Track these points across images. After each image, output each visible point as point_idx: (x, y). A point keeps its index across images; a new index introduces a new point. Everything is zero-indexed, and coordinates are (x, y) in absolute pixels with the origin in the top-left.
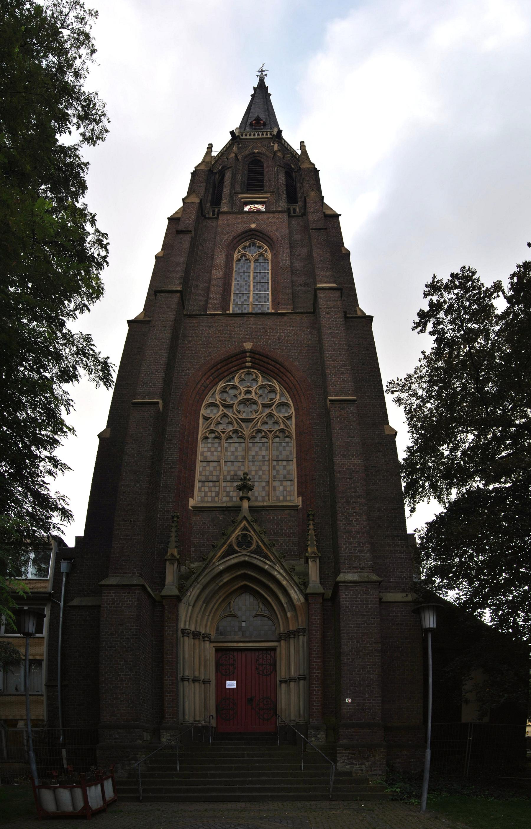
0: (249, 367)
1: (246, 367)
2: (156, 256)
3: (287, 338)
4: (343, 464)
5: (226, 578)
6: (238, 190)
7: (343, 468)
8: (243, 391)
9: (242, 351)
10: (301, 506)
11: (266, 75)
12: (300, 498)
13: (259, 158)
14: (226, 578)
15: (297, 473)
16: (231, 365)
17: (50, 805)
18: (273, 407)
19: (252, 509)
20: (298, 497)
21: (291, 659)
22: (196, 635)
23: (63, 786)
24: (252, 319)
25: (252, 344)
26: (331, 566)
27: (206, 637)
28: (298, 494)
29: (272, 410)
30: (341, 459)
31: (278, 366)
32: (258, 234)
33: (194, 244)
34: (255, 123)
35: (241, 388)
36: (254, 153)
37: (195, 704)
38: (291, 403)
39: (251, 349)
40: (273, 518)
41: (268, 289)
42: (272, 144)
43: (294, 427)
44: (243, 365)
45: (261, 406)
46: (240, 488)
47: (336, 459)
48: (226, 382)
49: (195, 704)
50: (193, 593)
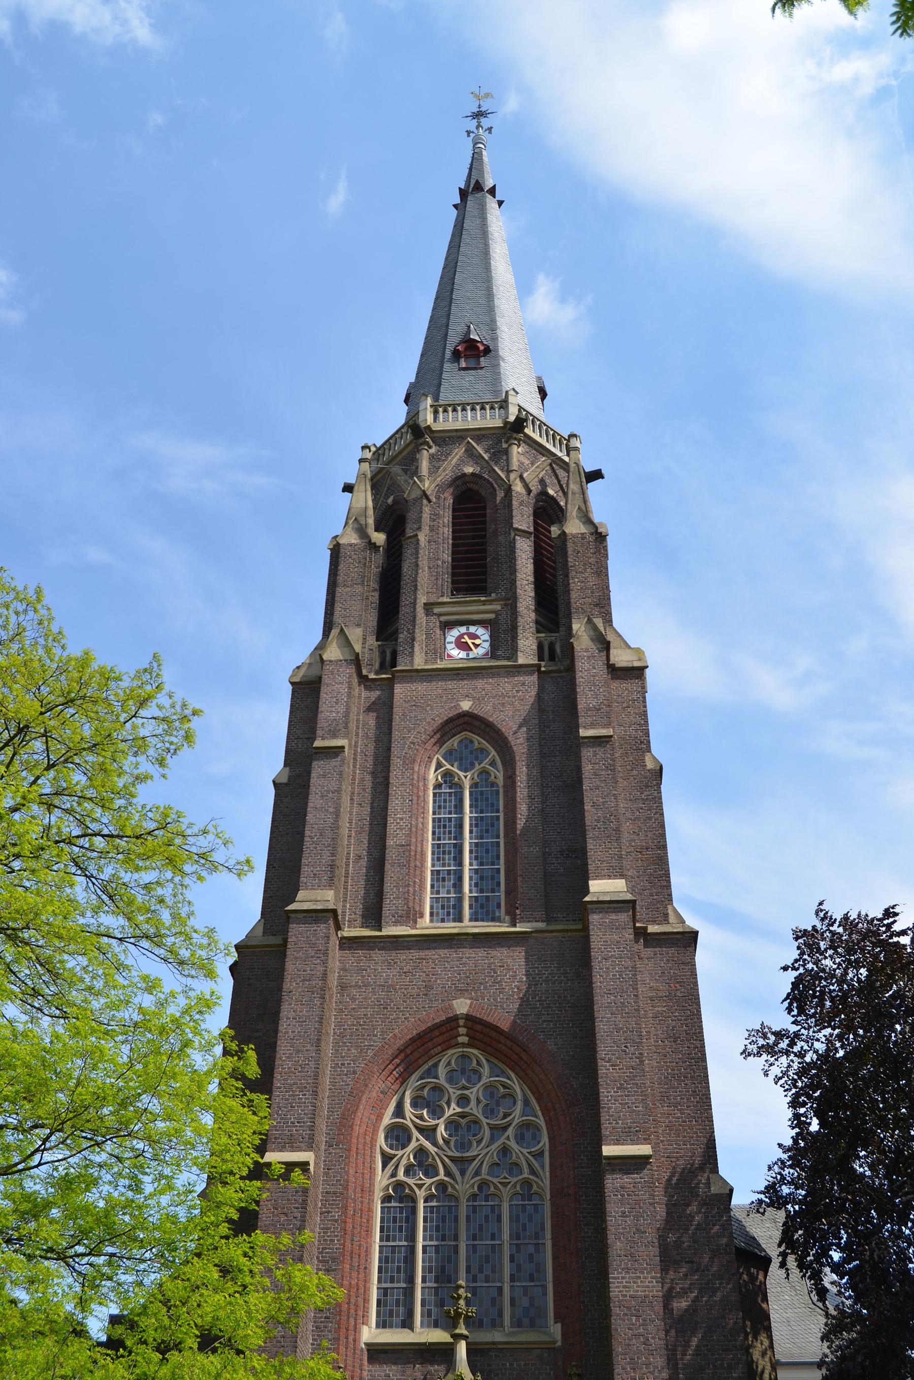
0: (463, 1045)
1: (457, 1045)
2: (274, 782)
4: (625, 1287)
7: (626, 1296)
8: (453, 1097)
9: (451, 1018)
10: (559, 1344)
11: (490, 129)
12: (559, 1325)
13: (475, 487)
15: (554, 1272)
16: (430, 1044)
18: (510, 1131)
20: (556, 1322)
25: (468, 1002)
28: (555, 1318)
29: (508, 1138)
30: (623, 1278)
31: (517, 1049)
32: (477, 723)
34: (466, 349)
35: (451, 1090)
36: (464, 475)
38: (542, 1122)
39: (467, 1015)
40: (511, 1365)
41: (498, 858)
42: (505, 446)
43: (548, 1174)
44: (453, 1042)
45: (486, 1128)
47: (614, 1278)
48: (421, 1078)
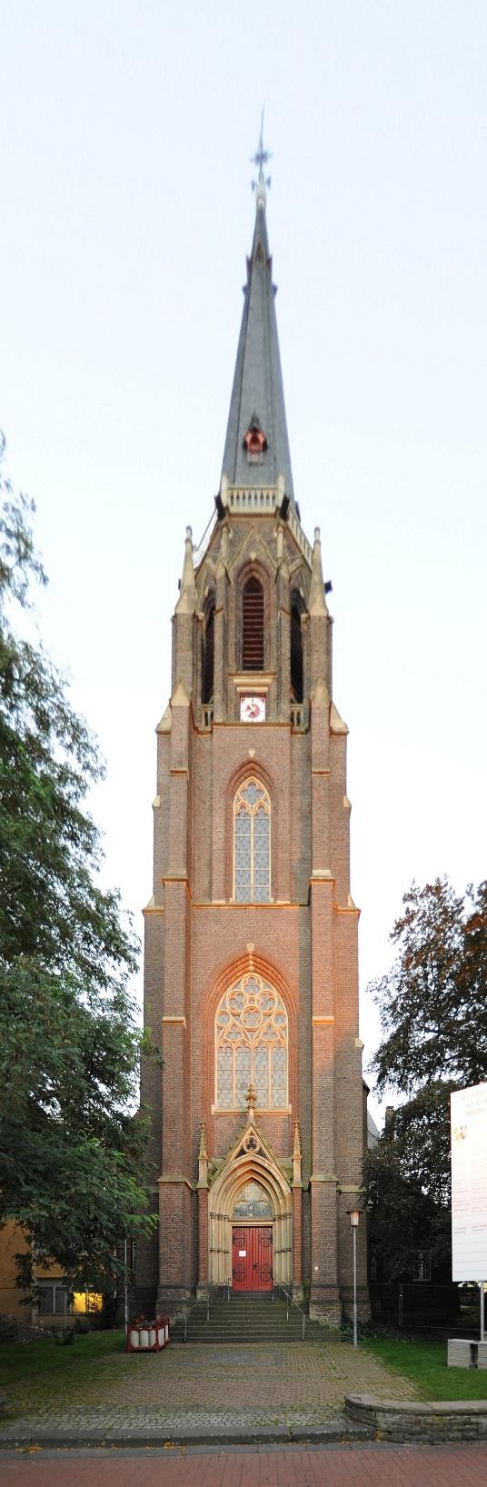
3: (283, 938)
5: (240, 1172)
6: (233, 669)
14: (240, 1172)
17: (135, 1344)
19: (257, 1117)
21: (282, 1234)
22: (219, 1217)
23: (145, 1328)
24: (276, 1447)
26: (307, 1167)
27: (226, 1218)
33: (190, 784)
37: (219, 1270)
46: (249, 1098)
49: (219, 1270)
50: (216, 1185)
